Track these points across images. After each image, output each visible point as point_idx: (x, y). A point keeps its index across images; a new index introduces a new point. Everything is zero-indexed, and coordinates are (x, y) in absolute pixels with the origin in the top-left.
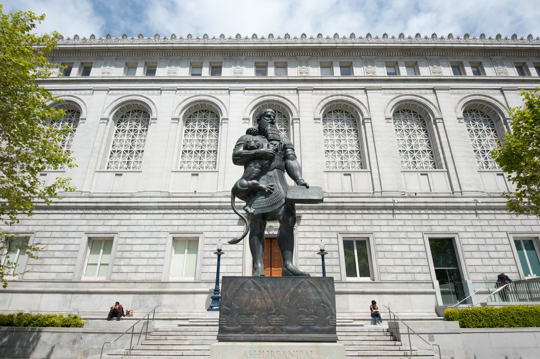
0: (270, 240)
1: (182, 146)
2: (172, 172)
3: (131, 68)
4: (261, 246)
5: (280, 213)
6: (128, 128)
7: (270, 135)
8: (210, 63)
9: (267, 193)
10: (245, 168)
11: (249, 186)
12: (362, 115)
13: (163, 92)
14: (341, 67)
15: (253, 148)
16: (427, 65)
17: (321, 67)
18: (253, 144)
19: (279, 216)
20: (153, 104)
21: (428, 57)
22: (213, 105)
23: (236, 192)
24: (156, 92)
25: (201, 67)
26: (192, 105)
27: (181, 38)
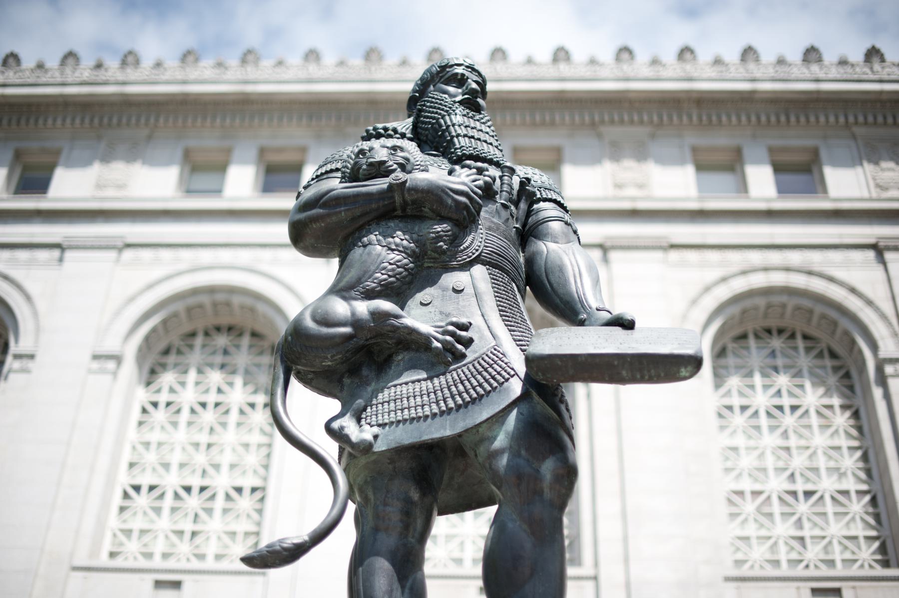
1: (124, 466)
2: (76, 569)
3: (204, 168)
5: (501, 440)
6: (188, 396)
8: (262, 151)
11: (356, 322)
12: (874, 346)
13: (69, 255)
14: (778, 169)
16: (855, 162)
17: (700, 168)
19: (499, 453)
20: (28, 297)
21: (858, 130)
22: (261, 308)
25: (221, 168)
26: (179, 306)
27: (40, 66)
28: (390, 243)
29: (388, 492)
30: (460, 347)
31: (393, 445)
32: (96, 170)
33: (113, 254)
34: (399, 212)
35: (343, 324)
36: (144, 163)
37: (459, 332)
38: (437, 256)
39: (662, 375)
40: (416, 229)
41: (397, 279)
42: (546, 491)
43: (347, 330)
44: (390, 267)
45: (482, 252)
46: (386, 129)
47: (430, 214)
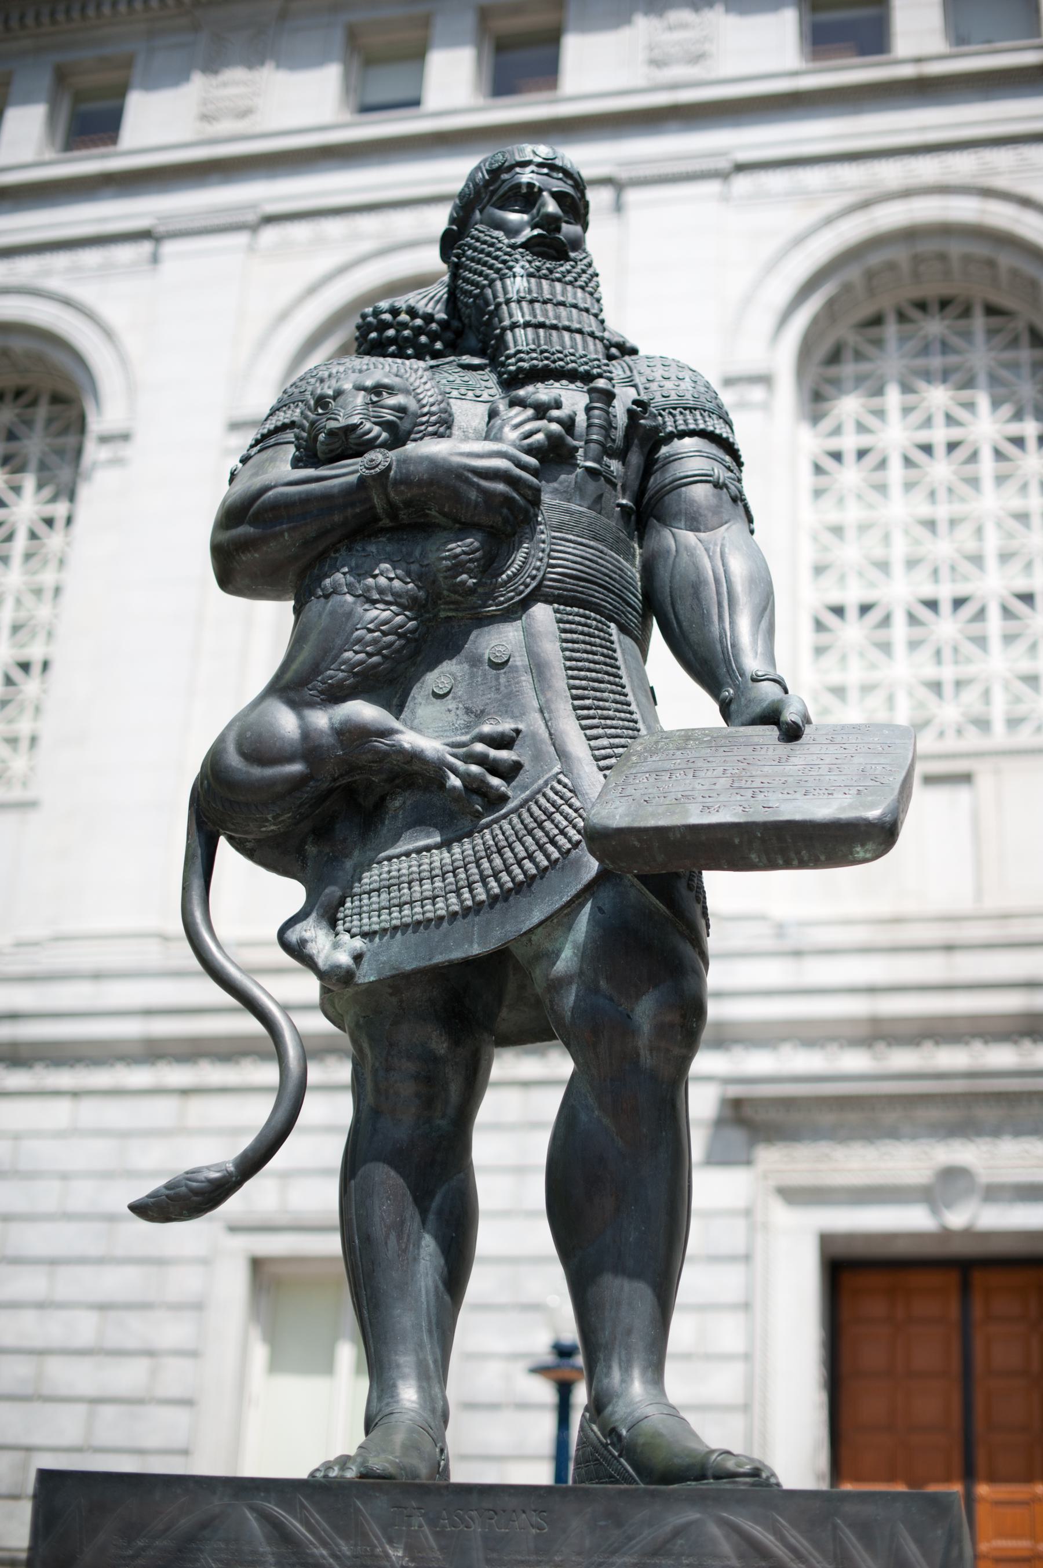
0: (953, 1278)
4: (429, 1244)
5: (567, 960)
7: (520, 340)
8: (484, 15)
9: (452, 802)
10: (297, 611)
11: (309, 748)
15: (348, 444)
18: (353, 411)
19: (557, 985)
20: (108, 333)
23: (227, 807)
24: (125, 253)
25: (417, 55)
28: (368, 589)
29: (391, 1045)
30: (495, 781)
31: (388, 973)
32: (198, 85)
33: (241, 239)
34: (386, 522)
35: (290, 759)
36: (278, 66)
37: (493, 753)
38: (460, 598)
39: (823, 858)
40: (417, 553)
41: (384, 656)
42: (644, 1053)
43: (296, 768)
44: (369, 636)
45: (544, 578)
46: (395, 312)
47: (441, 520)
